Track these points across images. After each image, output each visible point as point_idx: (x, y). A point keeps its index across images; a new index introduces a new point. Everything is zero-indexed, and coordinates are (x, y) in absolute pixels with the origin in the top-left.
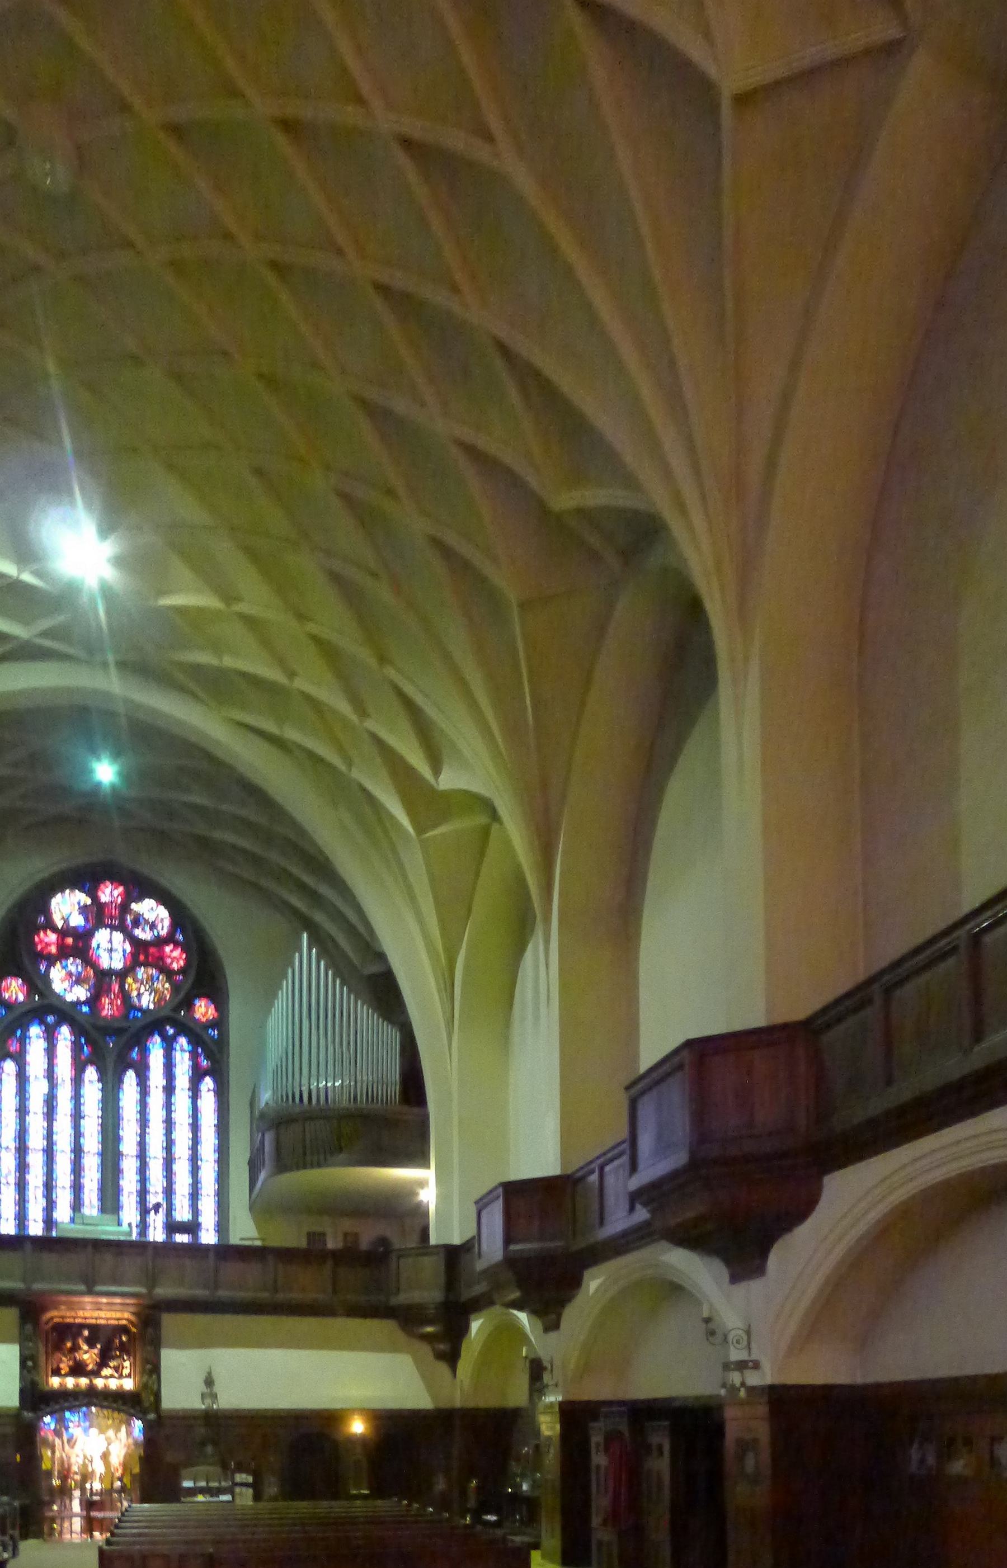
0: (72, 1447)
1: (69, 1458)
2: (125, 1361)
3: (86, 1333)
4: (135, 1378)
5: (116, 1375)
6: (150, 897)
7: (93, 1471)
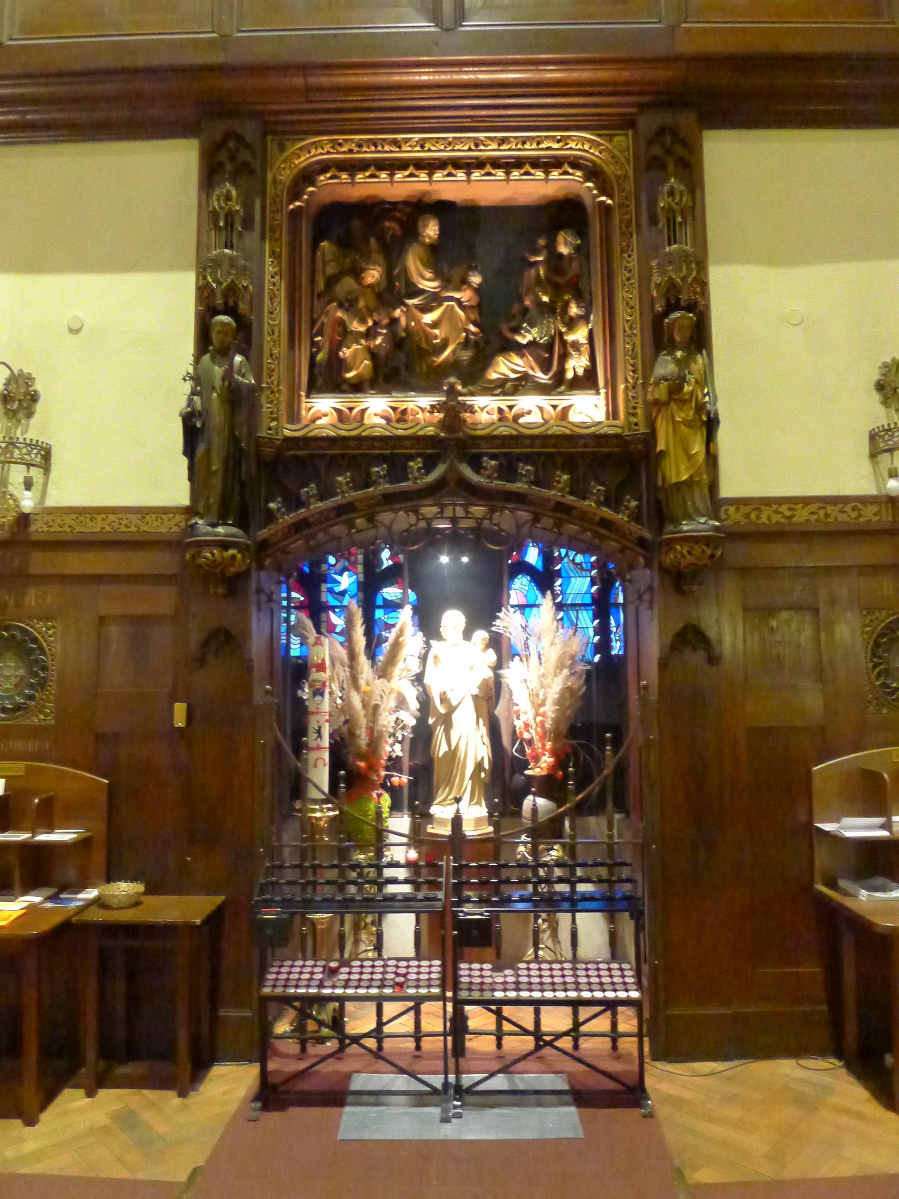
0: (384, 673)
1: (374, 711)
2: (571, 324)
3: (431, 230)
4: (612, 384)
5: (543, 378)
6: (467, 1023)
7: (452, 754)
